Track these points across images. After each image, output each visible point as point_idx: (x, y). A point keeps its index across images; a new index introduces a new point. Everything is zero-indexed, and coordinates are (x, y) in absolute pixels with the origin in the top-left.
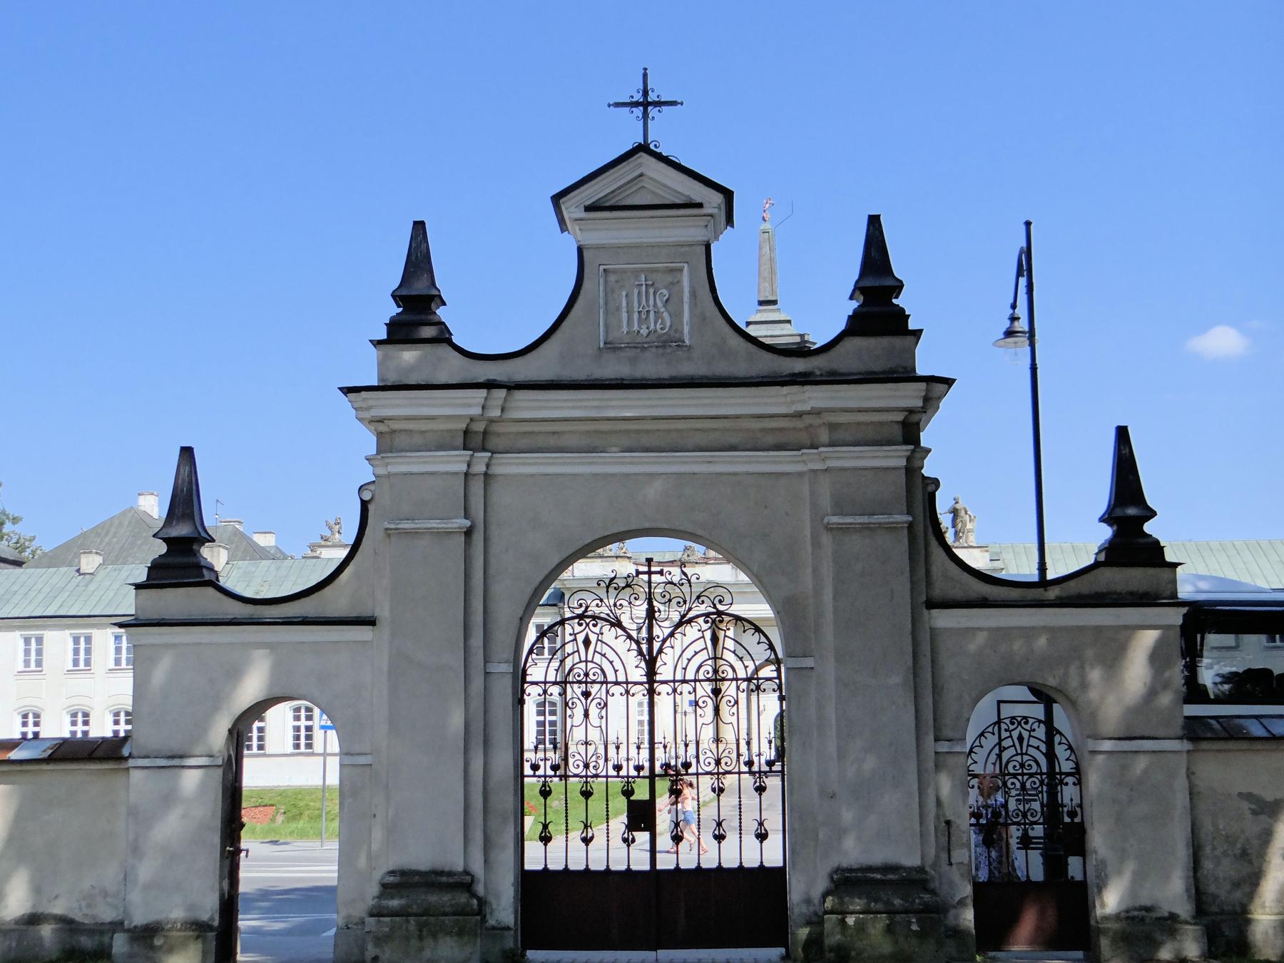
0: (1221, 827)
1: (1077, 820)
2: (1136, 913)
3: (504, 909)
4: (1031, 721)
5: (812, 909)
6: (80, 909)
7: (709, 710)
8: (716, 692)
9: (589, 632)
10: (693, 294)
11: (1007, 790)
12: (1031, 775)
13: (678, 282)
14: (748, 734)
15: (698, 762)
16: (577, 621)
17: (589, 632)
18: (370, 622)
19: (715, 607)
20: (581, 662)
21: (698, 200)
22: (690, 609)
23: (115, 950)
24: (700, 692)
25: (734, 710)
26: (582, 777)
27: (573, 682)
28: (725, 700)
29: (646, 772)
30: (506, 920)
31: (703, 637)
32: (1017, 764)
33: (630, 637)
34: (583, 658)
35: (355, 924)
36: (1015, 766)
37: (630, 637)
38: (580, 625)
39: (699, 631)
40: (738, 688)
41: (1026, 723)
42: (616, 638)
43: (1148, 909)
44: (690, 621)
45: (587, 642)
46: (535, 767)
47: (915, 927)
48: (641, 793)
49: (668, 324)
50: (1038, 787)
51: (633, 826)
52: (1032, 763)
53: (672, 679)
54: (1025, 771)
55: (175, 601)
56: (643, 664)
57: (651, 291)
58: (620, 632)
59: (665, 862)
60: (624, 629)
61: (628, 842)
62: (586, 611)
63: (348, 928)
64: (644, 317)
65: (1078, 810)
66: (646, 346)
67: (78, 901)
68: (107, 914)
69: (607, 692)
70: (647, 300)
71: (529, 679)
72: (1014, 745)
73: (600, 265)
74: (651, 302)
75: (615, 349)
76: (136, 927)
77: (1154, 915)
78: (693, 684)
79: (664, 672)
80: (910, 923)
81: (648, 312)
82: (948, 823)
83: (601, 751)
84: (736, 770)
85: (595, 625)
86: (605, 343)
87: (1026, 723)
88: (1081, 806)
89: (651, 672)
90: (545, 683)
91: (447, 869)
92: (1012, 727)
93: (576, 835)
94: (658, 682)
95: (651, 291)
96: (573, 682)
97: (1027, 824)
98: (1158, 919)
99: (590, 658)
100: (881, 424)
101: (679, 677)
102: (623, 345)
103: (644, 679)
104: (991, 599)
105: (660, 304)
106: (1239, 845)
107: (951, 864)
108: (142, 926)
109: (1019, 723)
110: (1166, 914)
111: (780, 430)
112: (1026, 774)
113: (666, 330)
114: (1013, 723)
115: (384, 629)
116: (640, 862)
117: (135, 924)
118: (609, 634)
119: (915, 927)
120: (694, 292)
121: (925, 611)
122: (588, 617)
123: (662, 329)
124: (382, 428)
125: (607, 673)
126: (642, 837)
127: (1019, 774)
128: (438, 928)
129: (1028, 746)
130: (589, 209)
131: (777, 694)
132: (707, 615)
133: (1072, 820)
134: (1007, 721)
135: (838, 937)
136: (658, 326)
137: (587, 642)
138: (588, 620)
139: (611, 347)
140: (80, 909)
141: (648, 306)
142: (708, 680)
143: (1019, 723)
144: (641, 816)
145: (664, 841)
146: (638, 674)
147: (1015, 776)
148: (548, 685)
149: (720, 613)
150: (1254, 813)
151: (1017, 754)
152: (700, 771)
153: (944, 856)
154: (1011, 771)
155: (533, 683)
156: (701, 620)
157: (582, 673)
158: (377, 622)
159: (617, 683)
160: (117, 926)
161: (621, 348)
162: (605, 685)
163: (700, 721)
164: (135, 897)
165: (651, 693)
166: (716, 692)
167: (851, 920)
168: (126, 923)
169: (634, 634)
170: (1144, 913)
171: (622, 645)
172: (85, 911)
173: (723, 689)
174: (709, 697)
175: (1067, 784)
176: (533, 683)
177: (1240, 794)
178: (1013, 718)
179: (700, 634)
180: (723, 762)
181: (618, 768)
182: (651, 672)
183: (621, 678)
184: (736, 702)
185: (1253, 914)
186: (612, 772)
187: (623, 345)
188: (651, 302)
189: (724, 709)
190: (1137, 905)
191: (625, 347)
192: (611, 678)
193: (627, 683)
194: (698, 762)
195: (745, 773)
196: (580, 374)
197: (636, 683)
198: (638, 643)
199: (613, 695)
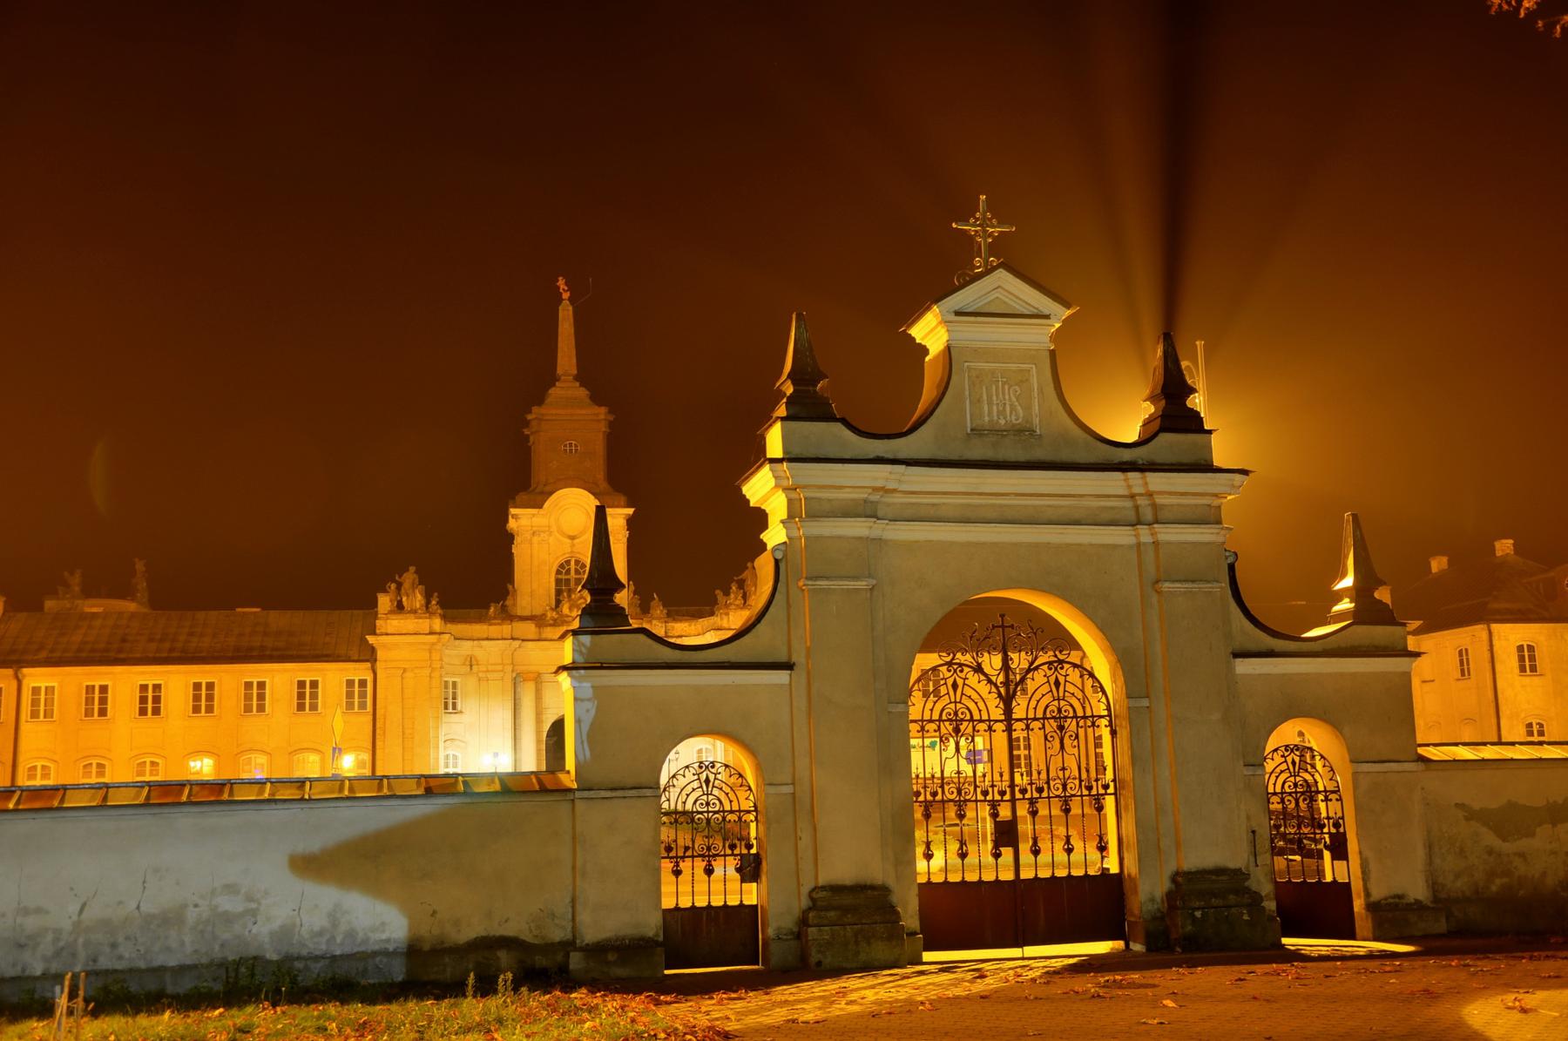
0: (1444, 830)
1: (754, 851)
2: (1392, 901)
3: (910, 917)
4: (718, 765)
5: (1156, 906)
6: (531, 931)
7: (1057, 741)
8: (1061, 728)
9: (957, 678)
10: (1041, 391)
11: (695, 825)
12: (715, 813)
13: (1027, 380)
14: (1088, 764)
15: (1049, 788)
16: (946, 667)
17: (957, 678)
18: (788, 666)
19: (1056, 656)
20: (951, 703)
21: (1046, 312)
22: (1036, 658)
23: (571, 967)
24: (1048, 729)
25: (1075, 743)
26: (1061, 797)
27: (945, 720)
28: (1067, 736)
29: (1007, 797)
30: (913, 926)
31: (1048, 682)
32: (1291, 784)
33: (990, 681)
34: (953, 700)
35: (785, 935)
36: (1290, 786)
37: (990, 681)
38: (1050, 669)
39: (1045, 676)
40: (1078, 723)
41: (713, 767)
42: (979, 682)
43: (1400, 897)
44: (1037, 668)
45: (1057, 683)
46: (1024, 791)
47: (1246, 917)
48: (1005, 813)
49: (1021, 415)
50: (720, 823)
51: (998, 844)
52: (717, 802)
53: (920, 718)
54: (710, 809)
55: (612, 644)
56: (1001, 705)
57: (1006, 387)
58: (982, 677)
59: (1026, 874)
60: (986, 675)
61: (997, 856)
62: (953, 659)
63: (779, 939)
64: (1001, 408)
65: (1341, 821)
66: (1005, 433)
67: (527, 923)
68: (557, 934)
69: (974, 727)
70: (1004, 394)
71: (1014, 716)
72: (1288, 769)
73: (1035, 364)
74: (1007, 397)
75: (981, 435)
76: (587, 945)
77: (1404, 901)
78: (937, 723)
79: (1019, 712)
80: (1242, 914)
81: (1005, 404)
82: (1253, 832)
83: (1076, 773)
84: (1079, 793)
85: (1062, 668)
86: (972, 430)
87: (713, 767)
88: (1343, 818)
89: (1008, 711)
90: (922, 721)
91: (869, 883)
92: (1286, 754)
93: (1059, 845)
94: (1014, 719)
95: (1006, 387)
96: (945, 720)
97: (711, 856)
98: (1407, 904)
99: (958, 700)
100: (1196, 505)
101: (1031, 715)
102: (986, 432)
103: (1003, 717)
104: (1276, 650)
105: (1014, 399)
106: (1457, 845)
107: (1257, 866)
108: (593, 944)
109: (1292, 751)
110: (1413, 901)
111: (1112, 508)
112: (711, 812)
113: (1020, 420)
114: (1287, 750)
115: (800, 675)
116: (1007, 875)
117: (586, 942)
118: (973, 679)
119: (1246, 917)
120: (1042, 390)
121: (1232, 660)
122: (956, 664)
123: (1016, 420)
124: (793, 495)
125: (1043, 708)
126: (1007, 853)
127: (1293, 792)
128: (870, 934)
129: (713, 787)
130: (958, 313)
131: (1109, 728)
132: (1050, 663)
133: (1337, 830)
134: (1283, 749)
135: (1190, 928)
136: (1013, 418)
137: (1057, 683)
138: (955, 667)
139: (977, 432)
140: (531, 931)
141: (1004, 399)
142: (1054, 718)
143: (707, 767)
144: (1006, 835)
145: (1026, 857)
146: (997, 713)
147: (1290, 794)
148: (925, 723)
149: (1061, 662)
150: (1467, 819)
151: (704, 794)
152: (1051, 795)
153: (1252, 859)
154: (1288, 790)
155: (1018, 720)
156: (1045, 667)
157: (952, 713)
158: (795, 668)
159: (981, 721)
160: (568, 946)
161: (984, 434)
162: (1074, 720)
163: (1049, 752)
164: (584, 917)
165: (1009, 730)
166: (1061, 728)
167: (1198, 914)
168: (578, 941)
169: (994, 679)
170: (1397, 900)
171: (984, 688)
172: (535, 933)
173: (1066, 725)
174: (1055, 732)
175: (1331, 800)
176: (1018, 720)
177: (1456, 804)
178: (1287, 746)
179: (1046, 680)
180: (1068, 787)
181: (985, 793)
182: (1008, 711)
183: (985, 717)
184: (1077, 737)
185: (791, 929)
186: (980, 797)
187: (986, 432)
188: (1007, 397)
189: (1067, 741)
190: (1392, 893)
191: (987, 434)
192: (977, 717)
193: (989, 720)
194: (1049, 788)
195: (1086, 795)
196: (954, 456)
197: (996, 721)
198: (997, 687)
199: (1032, 730)
